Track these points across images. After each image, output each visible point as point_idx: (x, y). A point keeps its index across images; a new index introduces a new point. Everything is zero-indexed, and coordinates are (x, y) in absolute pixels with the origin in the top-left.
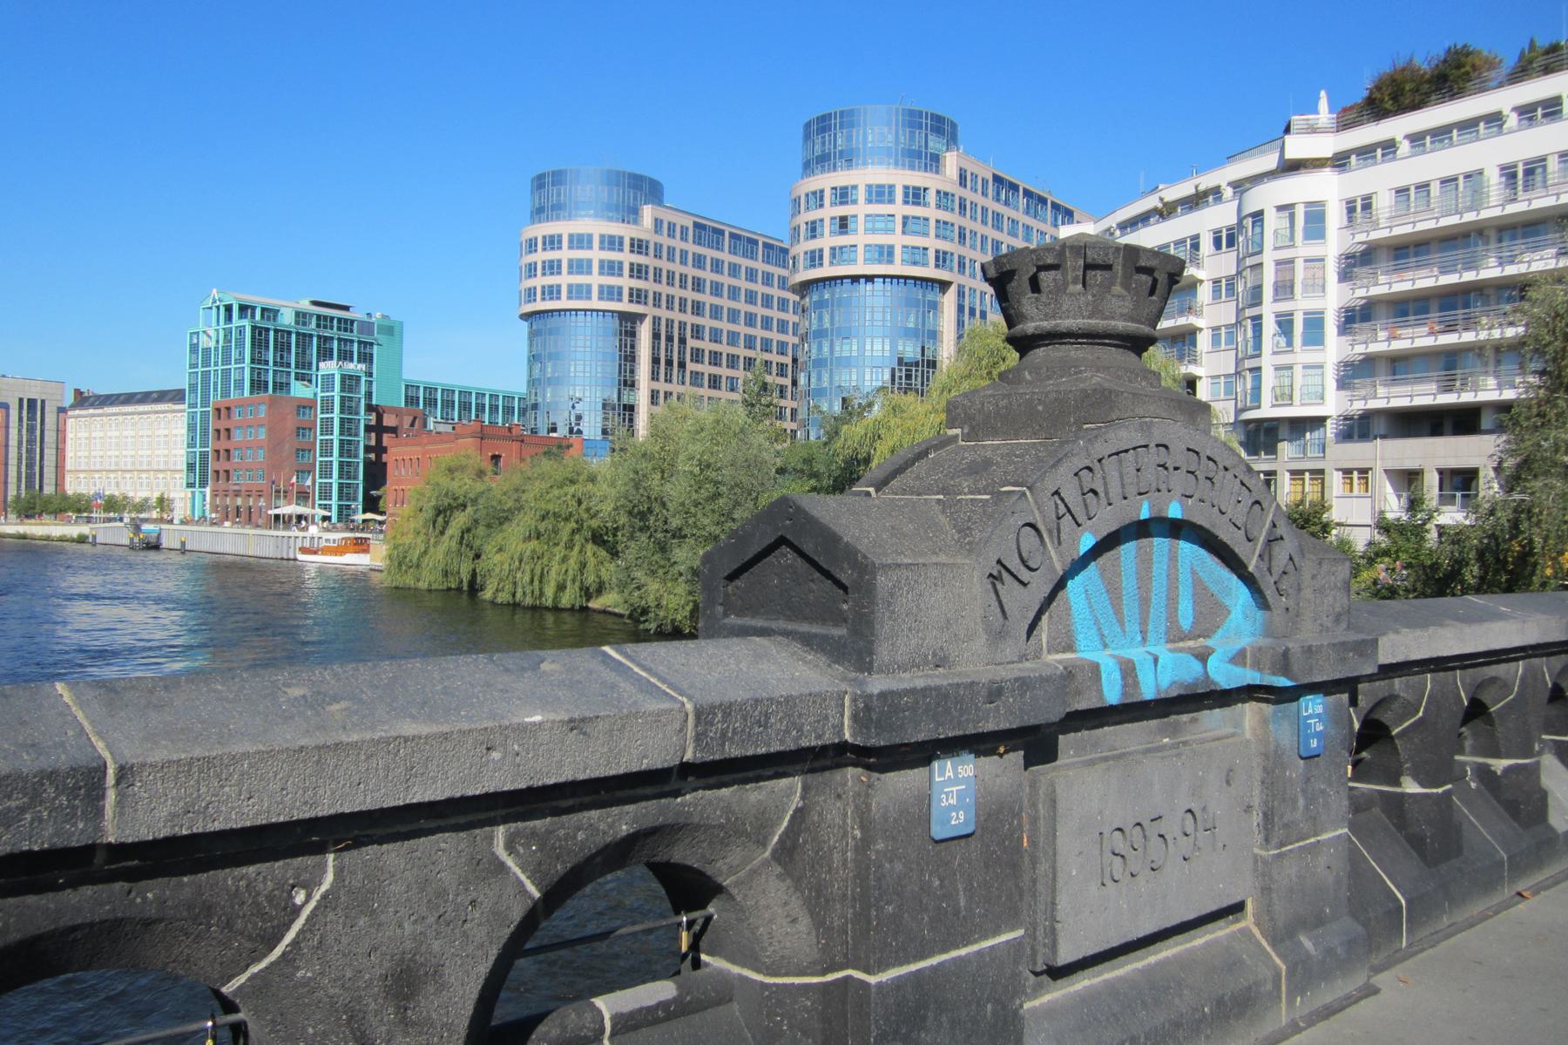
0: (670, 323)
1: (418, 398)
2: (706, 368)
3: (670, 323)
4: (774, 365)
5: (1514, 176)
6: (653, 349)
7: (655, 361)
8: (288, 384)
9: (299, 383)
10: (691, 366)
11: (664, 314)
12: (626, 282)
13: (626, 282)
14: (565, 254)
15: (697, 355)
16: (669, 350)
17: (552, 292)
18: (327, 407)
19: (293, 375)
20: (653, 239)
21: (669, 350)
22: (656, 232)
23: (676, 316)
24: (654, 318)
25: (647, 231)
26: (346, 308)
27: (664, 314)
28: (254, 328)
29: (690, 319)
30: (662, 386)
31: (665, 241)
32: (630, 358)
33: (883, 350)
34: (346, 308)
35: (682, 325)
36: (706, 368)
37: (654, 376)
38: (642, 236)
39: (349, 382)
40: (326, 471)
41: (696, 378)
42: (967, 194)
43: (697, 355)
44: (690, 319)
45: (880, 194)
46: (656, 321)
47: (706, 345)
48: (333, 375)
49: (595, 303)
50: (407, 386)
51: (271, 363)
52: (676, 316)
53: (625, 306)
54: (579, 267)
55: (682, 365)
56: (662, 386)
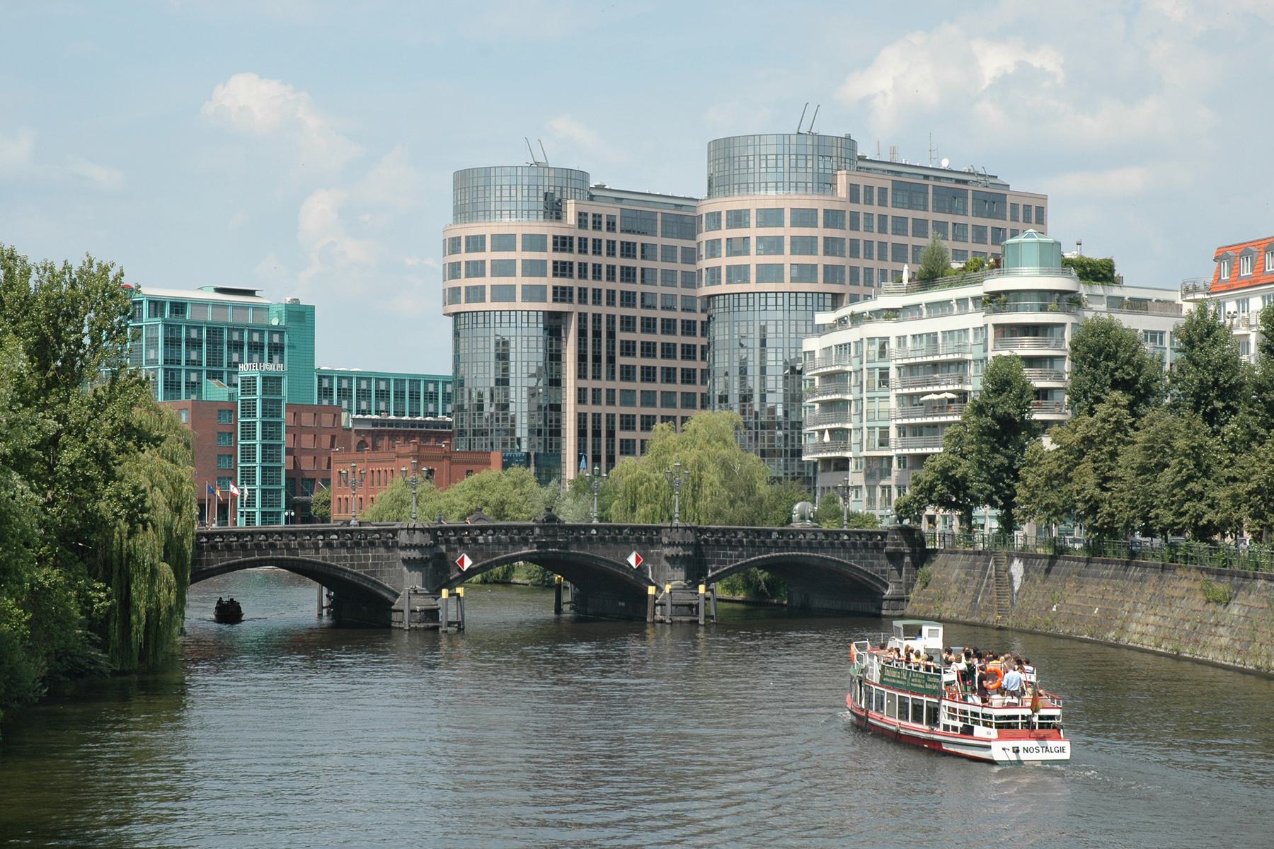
0: (597, 318)
1: (331, 389)
2: (638, 361)
3: (597, 318)
4: (970, 228)
5: (935, 340)
6: (580, 344)
7: (582, 358)
8: (200, 383)
9: (213, 382)
10: (620, 361)
11: (590, 309)
12: (550, 281)
13: (550, 281)
14: (488, 256)
15: (628, 349)
16: (597, 344)
17: (476, 294)
18: (249, 408)
19: (204, 374)
20: (577, 234)
21: (597, 344)
22: (580, 227)
23: (604, 310)
24: (580, 314)
25: (570, 227)
26: (251, 293)
27: (590, 309)
28: (166, 326)
29: (619, 311)
30: (590, 384)
31: (590, 234)
32: (555, 357)
33: (776, 360)
34: (251, 293)
35: (611, 319)
36: (638, 361)
37: (581, 375)
38: (566, 233)
39: (271, 382)
40: (248, 477)
41: (628, 373)
42: (861, 208)
43: (628, 349)
44: (619, 311)
45: (771, 217)
46: (582, 318)
47: (638, 337)
48: (254, 378)
49: (519, 304)
50: (320, 378)
51: (183, 363)
52: (604, 310)
53: (550, 306)
54: (503, 268)
55: (611, 360)
56: (590, 384)
